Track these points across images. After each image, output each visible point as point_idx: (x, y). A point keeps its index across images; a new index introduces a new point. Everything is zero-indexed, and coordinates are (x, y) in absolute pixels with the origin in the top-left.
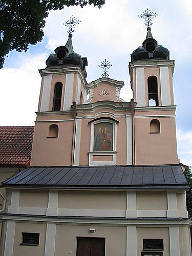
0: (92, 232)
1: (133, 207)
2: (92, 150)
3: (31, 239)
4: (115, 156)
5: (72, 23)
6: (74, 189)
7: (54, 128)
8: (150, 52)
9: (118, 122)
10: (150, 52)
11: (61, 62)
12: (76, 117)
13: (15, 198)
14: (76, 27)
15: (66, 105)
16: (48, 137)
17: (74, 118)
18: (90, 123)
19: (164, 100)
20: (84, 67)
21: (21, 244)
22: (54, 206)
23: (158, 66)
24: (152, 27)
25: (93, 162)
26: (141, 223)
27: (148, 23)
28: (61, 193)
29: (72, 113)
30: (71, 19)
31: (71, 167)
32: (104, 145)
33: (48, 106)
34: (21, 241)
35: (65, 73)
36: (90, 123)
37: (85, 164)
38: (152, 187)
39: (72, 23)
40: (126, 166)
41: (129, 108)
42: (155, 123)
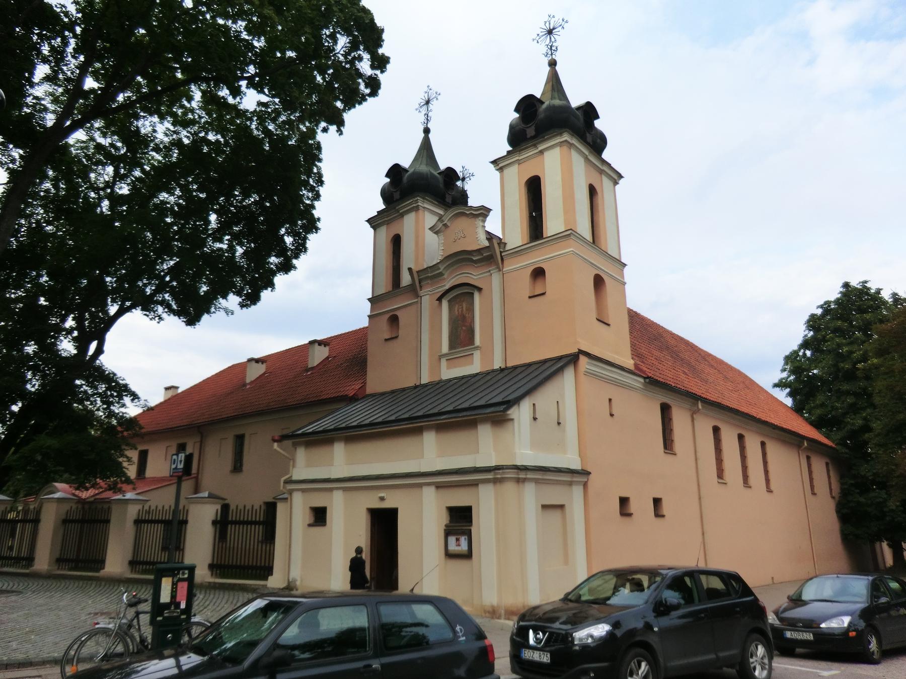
0: (382, 499)
1: (432, 452)
2: (445, 349)
3: (319, 516)
4: (477, 355)
5: (550, 32)
6: (321, 437)
7: (394, 320)
8: (549, 121)
9: (480, 290)
10: (549, 121)
11: (531, 132)
12: (421, 293)
13: (301, 454)
14: (560, 39)
15: (406, 279)
16: (386, 340)
17: (417, 296)
18: (440, 299)
19: (553, 225)
20: (591, 126)
21: (310, 525)
22: (340, 461)
23: (542, 152)
24: (558, 57)
25: (448, 372)
26: (445, 479)
27: (551, 49)
28: (441, 428)
29: (413, 290)
30: (547, 24)
31: (416, 387)
32: (462, 336)
33: (385, 287)
34: (312, 521)
35: (402, 215)
36: (440, 299)
37: (436, 379)
38: (468, 413)
39: (550, 32)
40: (493, 371)
41: (491, 254)
42: (539, 273)
